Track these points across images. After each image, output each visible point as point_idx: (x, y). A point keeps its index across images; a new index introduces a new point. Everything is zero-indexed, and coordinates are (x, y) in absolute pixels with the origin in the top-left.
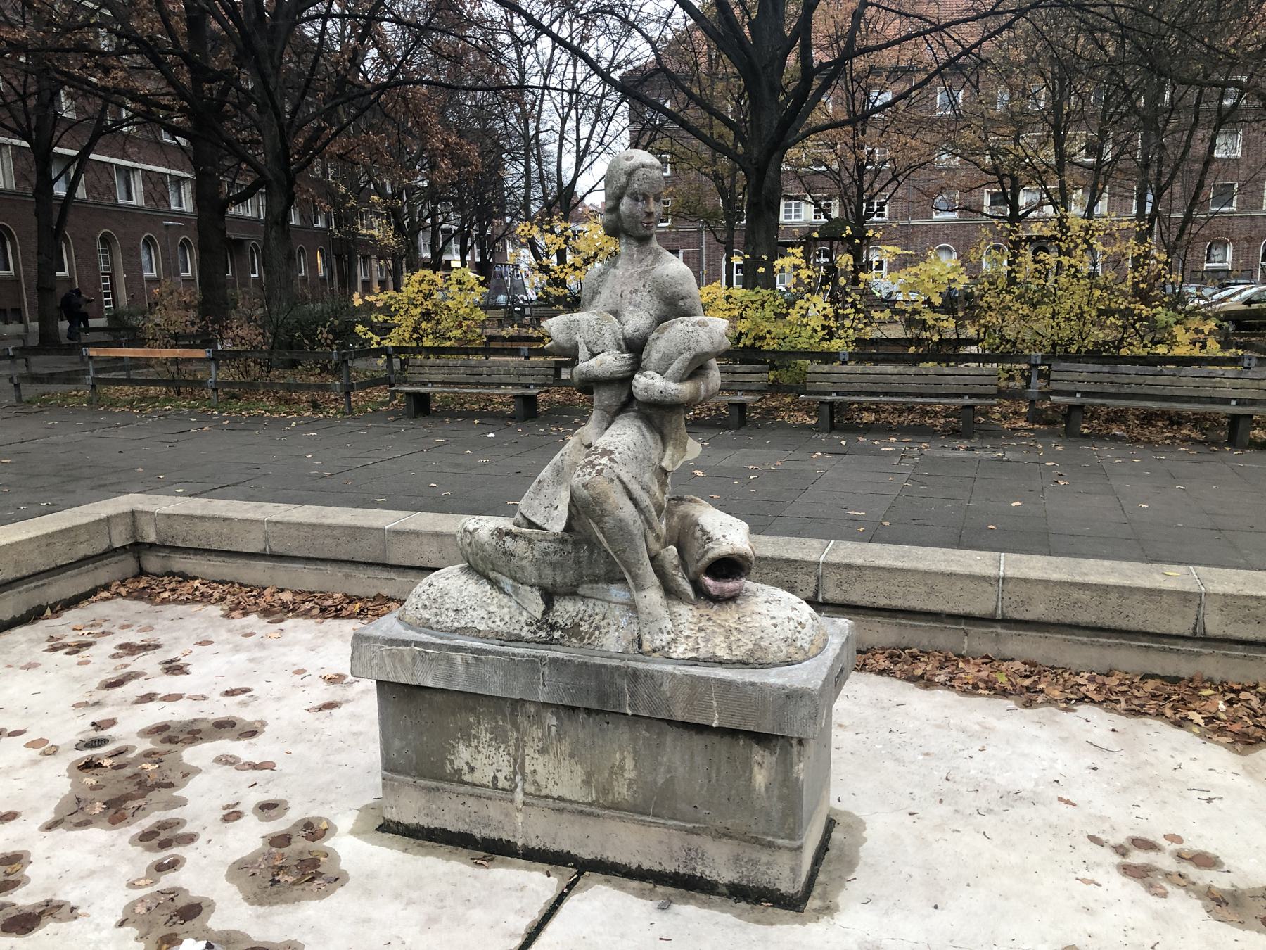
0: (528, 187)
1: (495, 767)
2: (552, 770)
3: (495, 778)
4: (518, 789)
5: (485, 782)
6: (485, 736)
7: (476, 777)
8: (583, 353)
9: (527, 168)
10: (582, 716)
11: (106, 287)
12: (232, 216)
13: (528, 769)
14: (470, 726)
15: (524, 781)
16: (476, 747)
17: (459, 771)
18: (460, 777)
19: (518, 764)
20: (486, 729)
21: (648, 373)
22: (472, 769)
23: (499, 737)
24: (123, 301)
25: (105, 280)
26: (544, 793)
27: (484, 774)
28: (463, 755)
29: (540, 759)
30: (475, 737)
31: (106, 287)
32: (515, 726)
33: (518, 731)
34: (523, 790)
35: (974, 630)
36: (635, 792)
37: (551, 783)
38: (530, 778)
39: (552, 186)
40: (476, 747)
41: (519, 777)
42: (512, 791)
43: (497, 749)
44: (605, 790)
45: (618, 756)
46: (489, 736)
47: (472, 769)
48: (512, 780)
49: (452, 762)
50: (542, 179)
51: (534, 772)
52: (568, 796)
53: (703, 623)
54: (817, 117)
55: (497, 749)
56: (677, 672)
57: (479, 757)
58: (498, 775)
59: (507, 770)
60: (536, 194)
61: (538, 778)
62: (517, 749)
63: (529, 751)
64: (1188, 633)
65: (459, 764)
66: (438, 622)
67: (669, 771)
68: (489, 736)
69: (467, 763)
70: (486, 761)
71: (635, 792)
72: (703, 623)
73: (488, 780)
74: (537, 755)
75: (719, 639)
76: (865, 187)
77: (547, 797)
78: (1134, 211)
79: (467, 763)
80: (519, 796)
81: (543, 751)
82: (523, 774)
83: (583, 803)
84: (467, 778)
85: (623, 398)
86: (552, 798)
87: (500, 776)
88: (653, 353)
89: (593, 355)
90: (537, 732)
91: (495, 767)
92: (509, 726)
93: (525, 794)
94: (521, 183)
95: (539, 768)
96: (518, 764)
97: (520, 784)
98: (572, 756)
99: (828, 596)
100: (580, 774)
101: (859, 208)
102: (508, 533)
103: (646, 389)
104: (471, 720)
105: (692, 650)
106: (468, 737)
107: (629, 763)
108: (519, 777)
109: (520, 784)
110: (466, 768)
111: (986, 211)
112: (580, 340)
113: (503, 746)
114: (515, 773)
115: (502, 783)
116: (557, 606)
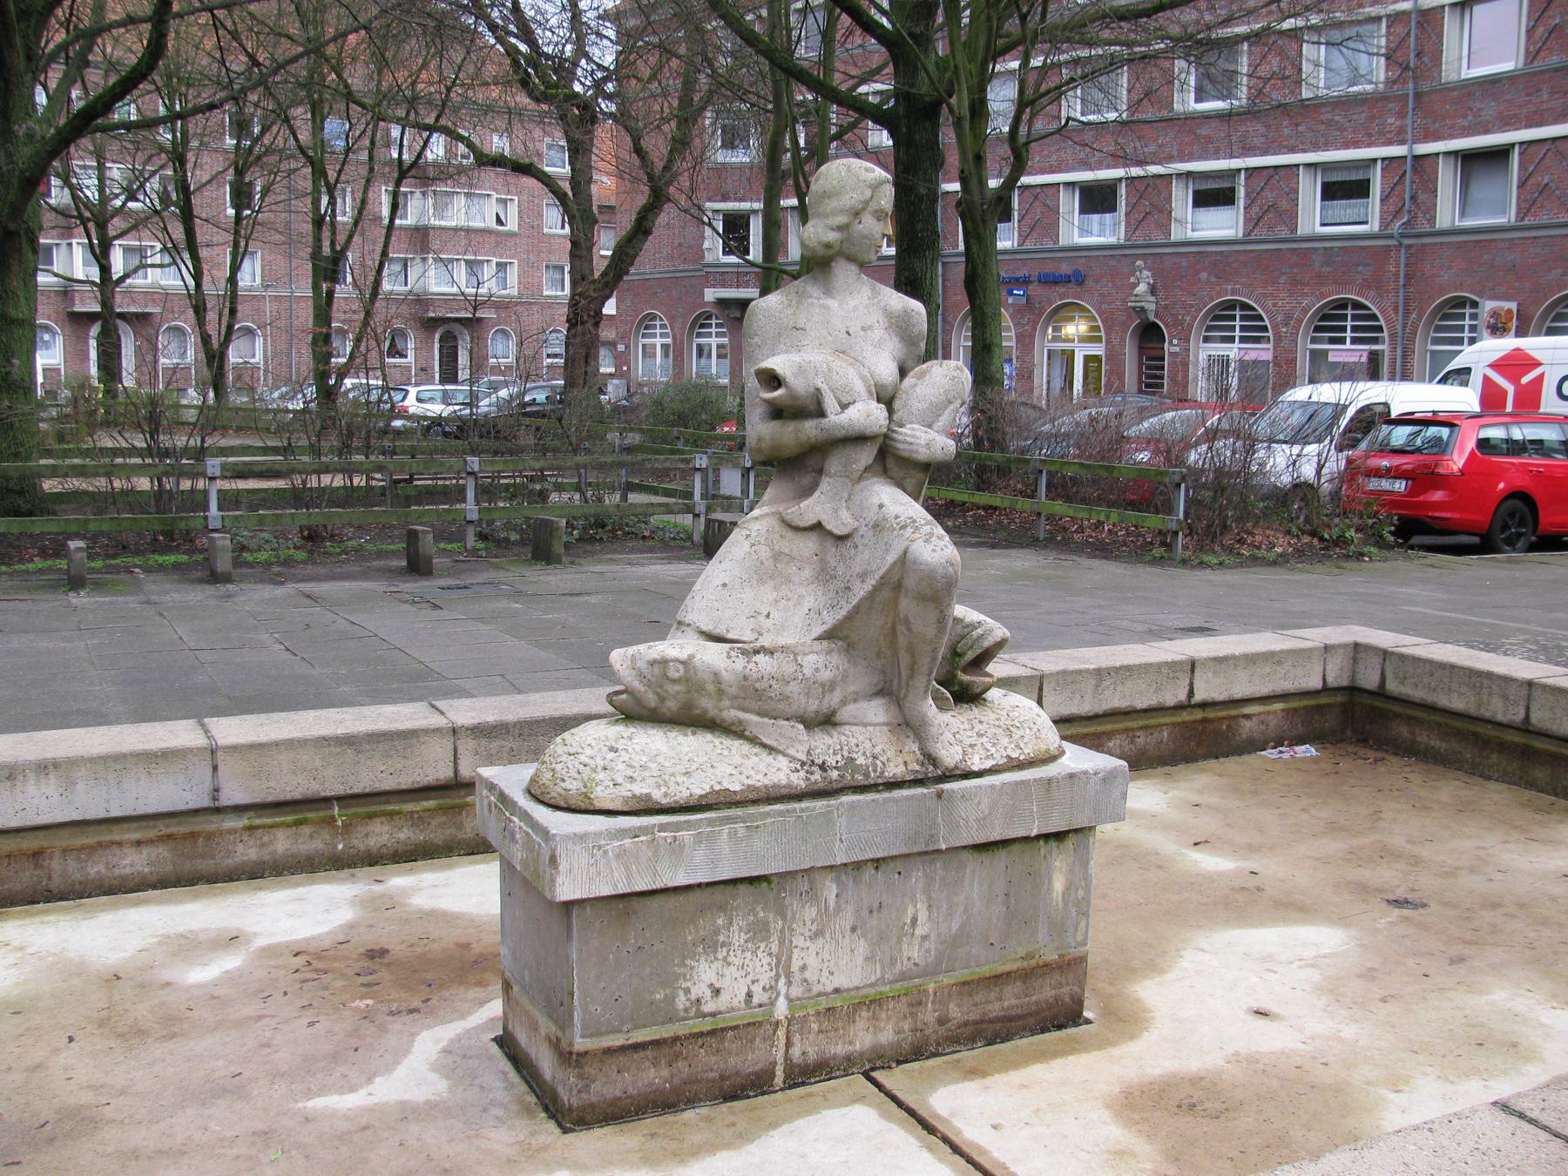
1: (750, 978)
2: (826, 957)
3: (749, 995)
6: (738, 938)
8: (831, 405)
10: (869, 871)
12: (758, 200)
14: (717, 932)
15: (789, 983)
22: (717, 992)
23: (759, 932)
29: (813, 948)
32: (781, 912)
33: (784, 918)
34: (787, 997)
35: (116, 828)
38: (797, 977)
40: (725, 959)
41: (782, 980)
43: (754, 953)
47: (717, 992)
49: (687, 991)
53: (978, 727)
55: (754, 953)
58: (753, 988)
59: (766, 977)
61: (807, 974)
62: (782, 943)
63: (799, 941)
64: (206, 802)
65: (700, 990)
66: (666, 795)
67: (966, 910)
70: (738, 974)
71: (928, 951)
72: (978, 727)
74: (808, 943)
75: (1005, 741)
78: (962, 247)
87: (756, 989)
89: (844, 407)
90: (810, 912)
91: (750, 978)
92: (771, 916)
95: (812, 961)
103: (928, 446)
104: (720, 922)
105: (987, 757)
106: (711, 945)
107: (923, 916)
108: (782, 980)
110: (708, 993)
112: (824, 387)
113: (763, 945)
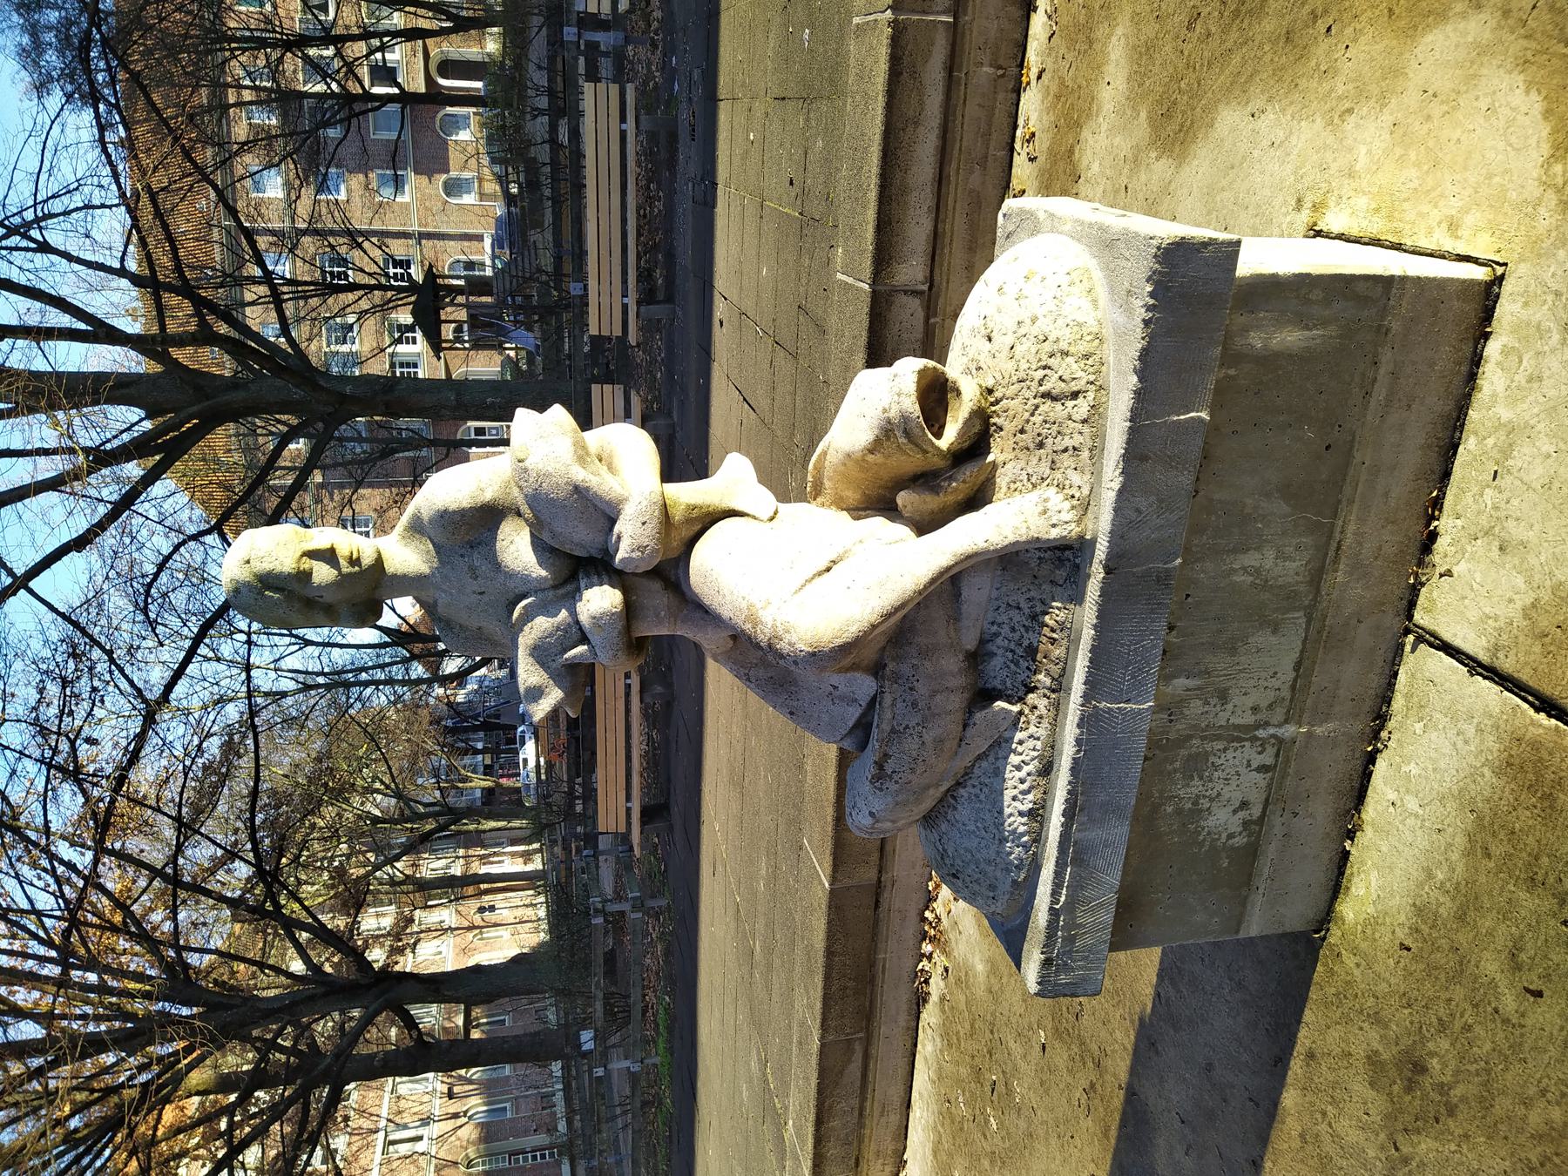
0: (390, 682)
1: (1242, 770)
2: (1252, 683)
4: (1280, 732)
5: (1263, 784)
6: (1196, 787)
7: (1256, 798)
9: (366, 684)
11: (525, 1160)
13: (1249, 719)
14: (1179, 812)
15: (1267, 724)
16: (1212, 800)
17: (1246, 824)
18: (1254, 822)
19: (1238, 735)
20: (1439, 905)
21: (307, 194)
22: (1244, 805)
24: (542, 1139)
25: (517, 1161)
26: (1286, 693)
27: (1252, 786)
28: (1223, 821)
29: (1236, 701)
30: (1195, 803)
31: (525, 1160)
33: (1190, 737)
34: (1280, 726)
36: (1298, 548)
37: (1274, 683)
39: (387, 656)
40: (1212, 800)
41: (1261, 733)
42: (1280, 741)
43: (1216, 767)
44: (1289, 597)
45: (1237, 578)
46: (1196, 782)
48: (1263, 743)
50: (382, 666)
51: (1255, 709)
52: (1295, 656)
54: (271, 332)
55: (1216, 767)
56: (1116, 485)
57: (1226, 795)
58: (1254, 765)
60: (397, 672)
61: (1264, 704)
62: (1218, 738)
65: (1235, 823)
68: (1196, 782)
69: (1235, 812)
70: (1234, 783)
73: (1261, 779)
74: (1230, 707)
76: (373, 282)
77: (1293, 688)
79: (1235, 812)
80: (1289, 731)
81: (1223, 696)
82: (1257, 726)
83: (1307, 630)
84: (1256, 812)
85: (657, 586)
86: (1295, 680)
87: (1257, 760)
88: (576, 538)
91: (1242, 770)
92: (1183, 752)
93: (1286, 721)
94: (388, 689)
95: (1249, 701)
96: (1238, 735)
97: (1272, 731)
98: (1233, 651)
99: (920, 276)
100: (1262, 638)
101: (399, 290)
102: (880, 765)
104: (1169, 809)
109: (1272, 731)
110: (1241, 814)
111: (394, 136)
113: (1212, 759)
114: (1255, 739)
115: (1267, 758)
116: (997, 684)
